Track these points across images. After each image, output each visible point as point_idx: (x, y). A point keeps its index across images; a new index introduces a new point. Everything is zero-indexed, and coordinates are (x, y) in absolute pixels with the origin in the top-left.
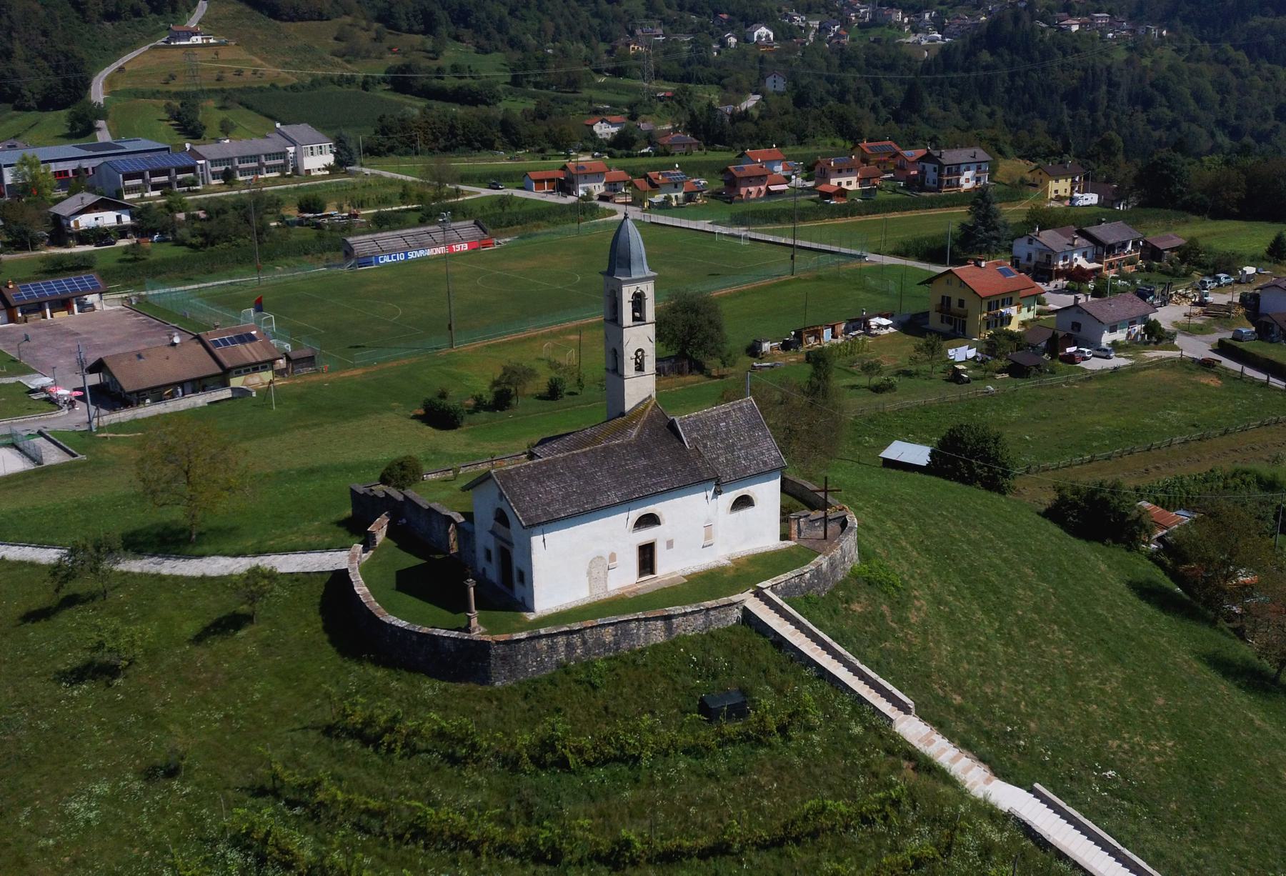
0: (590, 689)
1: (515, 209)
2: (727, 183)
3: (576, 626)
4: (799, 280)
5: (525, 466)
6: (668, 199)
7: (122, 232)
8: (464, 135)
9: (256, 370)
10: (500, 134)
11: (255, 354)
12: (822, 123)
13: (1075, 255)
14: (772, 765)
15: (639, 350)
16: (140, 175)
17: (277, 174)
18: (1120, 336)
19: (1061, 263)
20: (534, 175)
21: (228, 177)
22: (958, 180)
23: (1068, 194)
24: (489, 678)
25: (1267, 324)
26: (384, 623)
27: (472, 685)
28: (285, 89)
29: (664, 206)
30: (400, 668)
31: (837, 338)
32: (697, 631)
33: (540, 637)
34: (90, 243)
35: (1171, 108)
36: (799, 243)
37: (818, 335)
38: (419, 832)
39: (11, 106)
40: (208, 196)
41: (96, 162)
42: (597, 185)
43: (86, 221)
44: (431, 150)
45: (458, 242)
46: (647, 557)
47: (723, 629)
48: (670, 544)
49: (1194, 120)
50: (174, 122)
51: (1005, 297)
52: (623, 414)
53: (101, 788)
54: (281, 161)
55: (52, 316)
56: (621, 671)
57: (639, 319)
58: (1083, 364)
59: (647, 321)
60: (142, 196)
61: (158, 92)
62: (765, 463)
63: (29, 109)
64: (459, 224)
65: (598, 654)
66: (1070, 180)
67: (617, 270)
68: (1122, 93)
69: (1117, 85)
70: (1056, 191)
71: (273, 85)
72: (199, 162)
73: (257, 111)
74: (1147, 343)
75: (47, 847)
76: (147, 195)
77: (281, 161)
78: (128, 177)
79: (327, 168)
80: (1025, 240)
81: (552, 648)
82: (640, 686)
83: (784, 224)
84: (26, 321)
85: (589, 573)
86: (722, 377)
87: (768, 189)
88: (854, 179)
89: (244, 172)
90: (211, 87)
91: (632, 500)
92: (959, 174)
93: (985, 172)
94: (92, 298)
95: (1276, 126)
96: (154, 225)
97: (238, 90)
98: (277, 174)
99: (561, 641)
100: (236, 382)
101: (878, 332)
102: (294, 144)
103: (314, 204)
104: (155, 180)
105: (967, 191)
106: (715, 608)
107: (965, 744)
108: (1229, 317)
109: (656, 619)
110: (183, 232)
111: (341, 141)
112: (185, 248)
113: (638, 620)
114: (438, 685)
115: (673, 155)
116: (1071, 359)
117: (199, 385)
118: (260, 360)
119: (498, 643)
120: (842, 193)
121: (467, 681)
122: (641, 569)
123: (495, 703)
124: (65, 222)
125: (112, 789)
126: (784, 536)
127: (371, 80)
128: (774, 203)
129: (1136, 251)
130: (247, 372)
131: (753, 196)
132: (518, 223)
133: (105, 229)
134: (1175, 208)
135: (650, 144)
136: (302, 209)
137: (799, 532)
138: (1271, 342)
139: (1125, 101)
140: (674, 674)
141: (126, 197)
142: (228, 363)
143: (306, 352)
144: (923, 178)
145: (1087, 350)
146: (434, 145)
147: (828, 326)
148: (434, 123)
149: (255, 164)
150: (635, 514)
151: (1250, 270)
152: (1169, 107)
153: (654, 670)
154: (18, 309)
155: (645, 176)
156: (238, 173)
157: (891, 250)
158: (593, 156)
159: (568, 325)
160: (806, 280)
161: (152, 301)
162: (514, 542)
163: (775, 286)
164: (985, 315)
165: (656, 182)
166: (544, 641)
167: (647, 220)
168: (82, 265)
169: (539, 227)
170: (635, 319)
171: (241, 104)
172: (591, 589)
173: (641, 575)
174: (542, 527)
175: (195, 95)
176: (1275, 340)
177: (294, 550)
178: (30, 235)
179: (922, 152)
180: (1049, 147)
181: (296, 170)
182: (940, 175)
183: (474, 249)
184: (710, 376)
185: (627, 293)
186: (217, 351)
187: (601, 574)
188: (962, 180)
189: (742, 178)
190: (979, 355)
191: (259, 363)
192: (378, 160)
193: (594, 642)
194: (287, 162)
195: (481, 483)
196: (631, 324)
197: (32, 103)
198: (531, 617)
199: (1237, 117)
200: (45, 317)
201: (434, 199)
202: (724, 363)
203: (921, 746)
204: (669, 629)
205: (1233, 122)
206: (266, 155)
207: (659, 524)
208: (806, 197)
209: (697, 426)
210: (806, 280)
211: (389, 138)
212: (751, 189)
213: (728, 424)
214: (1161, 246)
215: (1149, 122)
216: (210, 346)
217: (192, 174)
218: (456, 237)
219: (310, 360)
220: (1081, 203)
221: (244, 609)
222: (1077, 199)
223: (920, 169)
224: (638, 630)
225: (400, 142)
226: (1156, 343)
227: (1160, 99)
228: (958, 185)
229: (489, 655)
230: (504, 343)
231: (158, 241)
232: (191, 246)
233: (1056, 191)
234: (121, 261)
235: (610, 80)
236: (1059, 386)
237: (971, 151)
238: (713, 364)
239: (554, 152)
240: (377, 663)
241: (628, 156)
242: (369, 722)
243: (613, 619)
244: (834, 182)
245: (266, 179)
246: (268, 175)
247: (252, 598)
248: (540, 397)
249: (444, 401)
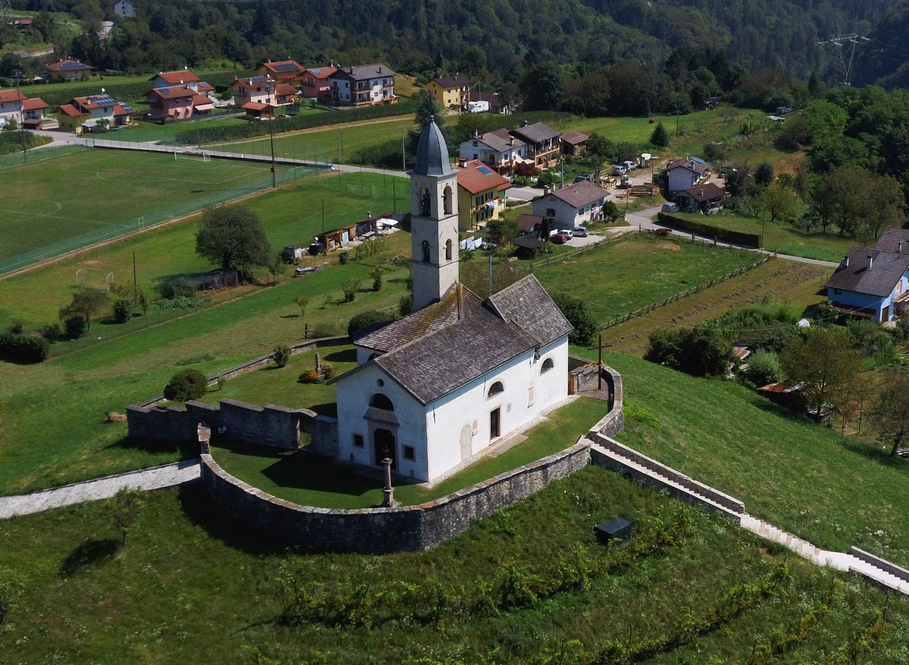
0: (507, 537)
2: (153, 105)
4: (282, 191)
12: (208, 46)
13: (513, 154)
14: (679, 569)
15: (424, 242)
18: (586, 217)
19: (503, 161)
22: (369, 94)
23: (458, 103)
24: (419, 544)
25: (684, 198)
27: (404, 554)
29: (98, 131)
30: (330, 552)
32: (563, 476)
33: (457, 499)
35: (481, 24)
36: (277, 159)
37: (338, 239)
48: (509, 407)
49: (501, 35)
51: (487, 192)
52: (438, 300)
56: (524, 518)
58: (568, 243)
66: (459, 90)
67: (430, 169)
68: (439, 14)
69: (434, 6)
70: (449, 101)
74: (606, 222)
80: (470, 144)
81: (467, 507)
82: (544, 527)
83: (229, 141)
85: (461, 441)
86: (272, 284)
87: (194, 109)
88: (272, 97)
92: (368, 88)
93: (390, 86)
95: (567, 39)
101: (385, 232)
105: (377, 105)
108: (651, 195)
109: (537, 469)
115: (69, 81)
116: (558, 240)
119: (427, 510)
120: (269, 110)
121: (397, 550)
122: (492, 432)
126: (570, 392)
128: (205, 122)
129: (557, 147)
131: (181, 117)
134: (556, 110)
138: (690, 212)
139: (442, 20)
144: (336, 93)
145: (569, 231)
147: (345, 230)
151: (647, 156)
152: (479, 25)
155: (73, 102)
157: (348, 159)
160: (288, 191)
162: (400, 421)
163: (262, 197)
164: (474, 209)
165: (86, 107)
166: (461, 503)
167: (91, 144)
172: (462, 456)
176: (693, 210)
177: (102, 475)
179: (332, 69)
180: (422, 62)
182: (353, 89)
184: (259, 285)
185: (441, 188)
188: (372, 94)
189: (168, 100)
190: (485, 243)
193: (496, 497)
195: (348, 375)
199: (535, 32)
202: (273, 272)
205: (532, 37)
208: (232, 115)
210: (288, 191)
212: (179, 110)
214: (572, 141)
215: (465, 38)
220: (476, 110)
221: (113, 535)
222: (473, 107)
223: (332, 84)
226: (613, 221)
227: (471, 18)
228: (369, 99)
229: (419, 522)
230: (25, 275)
233: (449, 101)
236: (561, 262)
237: (376, 67)
238: (257, 272)
240: (303, 552)
242: (331, 604)
243: (506, 475)
244: (254, 99)
247: (120, 522)
248: (105, 322)
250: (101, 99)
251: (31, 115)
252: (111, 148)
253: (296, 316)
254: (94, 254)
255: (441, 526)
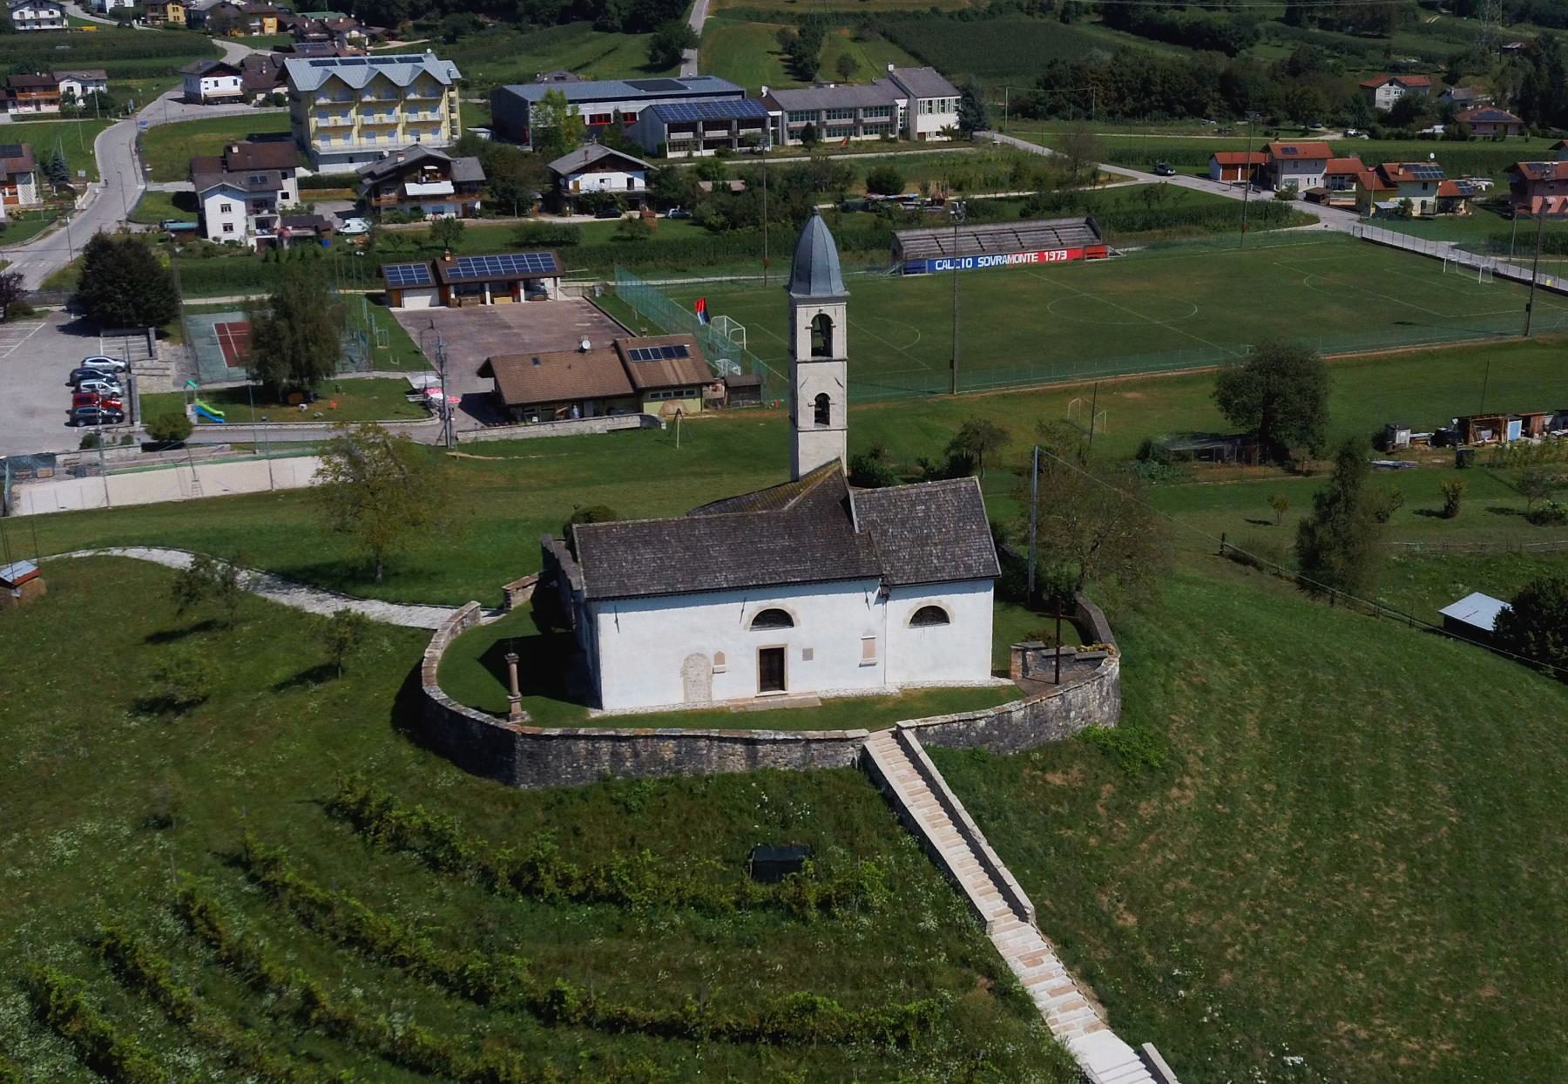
1: (1168, 204)
3: (625, 732)
4: (1533, 344)
5: (621, 526)
6: (1407, 205)
7: (632, 200)
8: (1162, 93)
9: (679, 395)
10: (1217, 95)
11: (679, 372)
16: (691, 127)
17: (876, 137)
20: (1222, 158)
21: (809, 136)
26: (423, 691)
28: (951, 16)
29: (1400, 216)
31: (1531, 436)
32: (791, 767)
33: (578, 737)
34: (590, 213)
37: (1497, 427)
38: (356, 938)
39: (589, 24)
40: (792, 159)
41: (644, 105)
42: (1312, 177)
43: (589, 182)
44: (1111, 113)
45: (1053, 247)
46: (772, 667)
47: (828, 772)
48: (808, 655)
50: (787, 56)
53: (90, 827)
54: (887, 119)
55: (492, 302)
57: (822, 351)
59: (835, 356)
60: (690, 155)
61: (778, 13)
62: (968, 568)
63: (612, 30)
64: (1063, 222)
65: (653, 773)
71: (934, 10)
72: (772, 113)
73: (902, 47)
75: (13, 877)
76: (696, 154)
77: (887, 119)
78: (675, 128)
79: (946, 131)
81: (593, 755)
84: (460, 305)
85: (684, 673)
86: (1309, 473)
89: (832, 131)
90: (850, 10)
91: (748, 587)
94: (548, 283)
96: (672, 195)
97: (885, 14)
98: (876, 137)
99: (605, 747)
100: (652, 408)
102: (907, 94)
103: (888, 183)
104: (710, 134)
106: (819, 741)
107: (1087, 975)
109: (735, 740)
110: (704, 208)
111: (968, 95)
112: (701, 229)
113: (708, 738)
114: (458, 774)
115: (1473, 139)
117: (603, 405)
118: (684, 382)
119: (524, 735)
121: (491, 778)
122: (762, 681)
123: (510, 808)
124: (562, 182)
125: (101, 830)
126: (1000, 671)
127: (1073, 7)
130: (667, 396)
132: (1159, 226)
133: (611, 196)
135: (1445, 120)
136: (874, 186)
137: (1025, 669)
140: (736, 813)
141: (670, 155)
142: (642, 382)
143: (752, 380)
146: (1117, 107)
147: (1516, 417)
148: (1122, 74)
149: (850, 121)
150: (754, 607)
153: (712, 803)
154: (452, 288)
156: (824, 132)
158: (1346, 134)
159: (1131, 377)
160: (1545, 346)
161: (619, 295)
163: (1491, 348)
165: (1393, 178)
166: (582, 744)
168: (564, 240)
169: (1189, 233)
170: (815, 352)
171: (884, 35)
173: (763, 688)
174: (615, 602)
175: (821, 20)
178: (518, 196)
181: (905, 133)
183: (1075, 260)
185: (805, 316)
186: (633, 365)
187: (703, 677)
189: (1536, 182)
191: (673, 387)
192: (1032, 124)
194: (894, 120)
196: (810, 358)
197: (617, 22)
198: (595, 714)
200: (484, 302)
201: (1059, 185)
203: (1019, 968)
204: (752, 757)
206: (865, 109)
207: (792, 625)
209: (882, 505)
210: (1545, 346)
211: (1052, 95)
212: (1551, 199)
213: (928, 508)
216: (626, 355)
217: (759, 130)
218: (1053, 239)
219: (753, 390)
224: (709, 751)
225: (1069, 100)
229: (514, 749)
230: (1032, 394)
231: (674, 217)
232: (710, 227)
234: (614, 239)
235: (1445, 19)
238: (1298, 452)
239: (1289, 124)
241: (1399, 137)
245: (859, 143)
246: (865, 138)
249: (872, 461)
250: (1425, 169)
251: (1338, 181)
252: (1402, 249)
253: (1267, 523)
254: (1142, 385)
255: (547, 765)
